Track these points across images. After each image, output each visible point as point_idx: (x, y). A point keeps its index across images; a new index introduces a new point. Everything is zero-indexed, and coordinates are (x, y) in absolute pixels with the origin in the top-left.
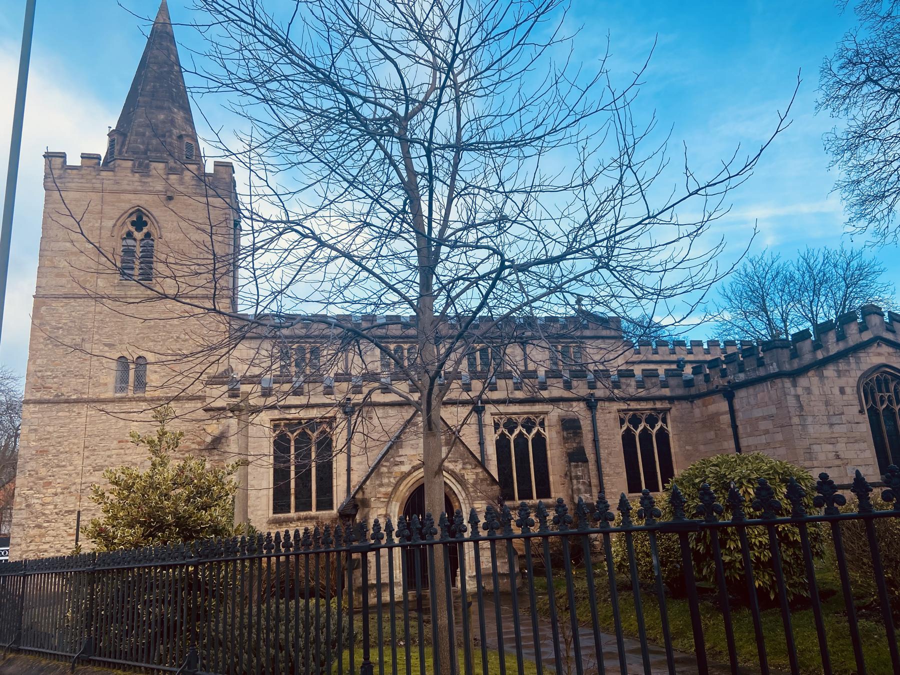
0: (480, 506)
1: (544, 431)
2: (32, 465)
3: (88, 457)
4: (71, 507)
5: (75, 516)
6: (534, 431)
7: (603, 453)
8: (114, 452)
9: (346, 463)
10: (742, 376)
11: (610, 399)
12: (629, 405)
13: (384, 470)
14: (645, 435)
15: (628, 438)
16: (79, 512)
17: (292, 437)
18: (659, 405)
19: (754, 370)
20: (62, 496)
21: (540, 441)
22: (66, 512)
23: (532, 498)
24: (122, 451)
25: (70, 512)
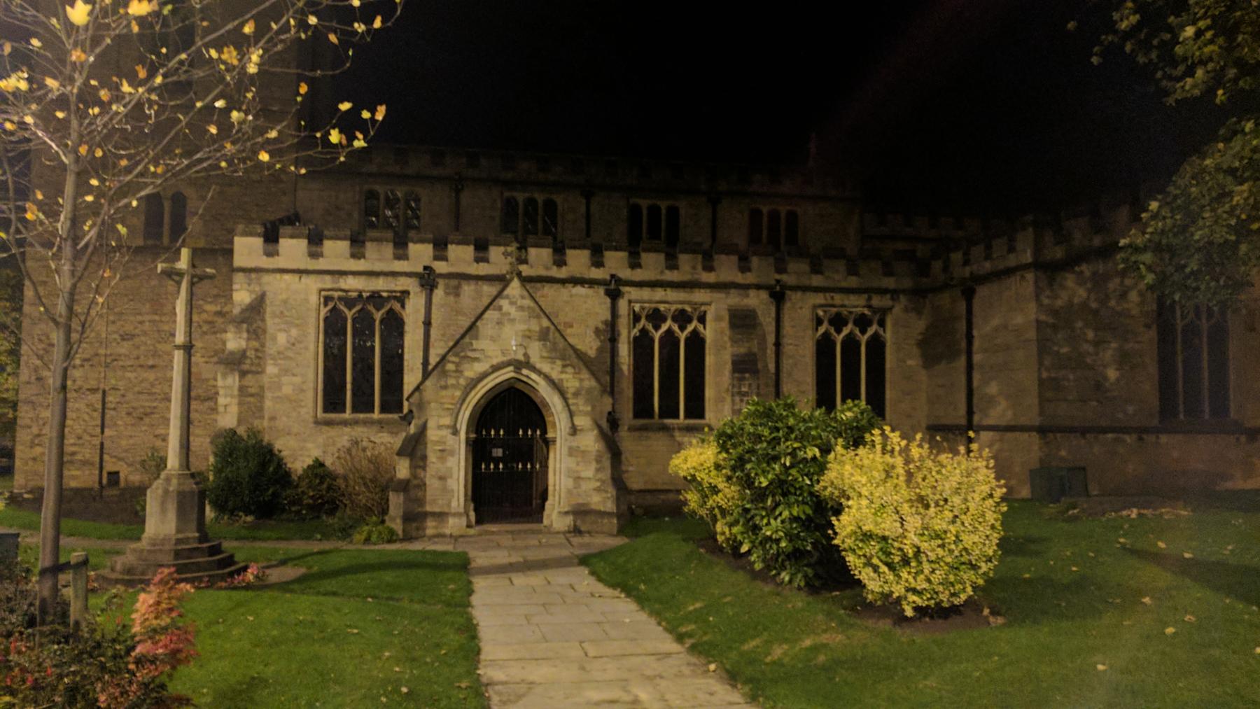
0: (583, 423)
2: (37, 330)
3: (113, 322)
4: (93, 384)
5: (99, 396)
6: (690, 328)
7: (786, 364)
8: (147, 318)
9: (421, 354)
10: (988, 265)
13: (450, 367)
15: (824, 348)
16: (104, 392)
17: (349, 314)
18: (877, 301)
20: (81, 369)
21: (696, 343)
22: (88, 390)
23: (677, 417)
24: (157, 318)
25: (93, 391)
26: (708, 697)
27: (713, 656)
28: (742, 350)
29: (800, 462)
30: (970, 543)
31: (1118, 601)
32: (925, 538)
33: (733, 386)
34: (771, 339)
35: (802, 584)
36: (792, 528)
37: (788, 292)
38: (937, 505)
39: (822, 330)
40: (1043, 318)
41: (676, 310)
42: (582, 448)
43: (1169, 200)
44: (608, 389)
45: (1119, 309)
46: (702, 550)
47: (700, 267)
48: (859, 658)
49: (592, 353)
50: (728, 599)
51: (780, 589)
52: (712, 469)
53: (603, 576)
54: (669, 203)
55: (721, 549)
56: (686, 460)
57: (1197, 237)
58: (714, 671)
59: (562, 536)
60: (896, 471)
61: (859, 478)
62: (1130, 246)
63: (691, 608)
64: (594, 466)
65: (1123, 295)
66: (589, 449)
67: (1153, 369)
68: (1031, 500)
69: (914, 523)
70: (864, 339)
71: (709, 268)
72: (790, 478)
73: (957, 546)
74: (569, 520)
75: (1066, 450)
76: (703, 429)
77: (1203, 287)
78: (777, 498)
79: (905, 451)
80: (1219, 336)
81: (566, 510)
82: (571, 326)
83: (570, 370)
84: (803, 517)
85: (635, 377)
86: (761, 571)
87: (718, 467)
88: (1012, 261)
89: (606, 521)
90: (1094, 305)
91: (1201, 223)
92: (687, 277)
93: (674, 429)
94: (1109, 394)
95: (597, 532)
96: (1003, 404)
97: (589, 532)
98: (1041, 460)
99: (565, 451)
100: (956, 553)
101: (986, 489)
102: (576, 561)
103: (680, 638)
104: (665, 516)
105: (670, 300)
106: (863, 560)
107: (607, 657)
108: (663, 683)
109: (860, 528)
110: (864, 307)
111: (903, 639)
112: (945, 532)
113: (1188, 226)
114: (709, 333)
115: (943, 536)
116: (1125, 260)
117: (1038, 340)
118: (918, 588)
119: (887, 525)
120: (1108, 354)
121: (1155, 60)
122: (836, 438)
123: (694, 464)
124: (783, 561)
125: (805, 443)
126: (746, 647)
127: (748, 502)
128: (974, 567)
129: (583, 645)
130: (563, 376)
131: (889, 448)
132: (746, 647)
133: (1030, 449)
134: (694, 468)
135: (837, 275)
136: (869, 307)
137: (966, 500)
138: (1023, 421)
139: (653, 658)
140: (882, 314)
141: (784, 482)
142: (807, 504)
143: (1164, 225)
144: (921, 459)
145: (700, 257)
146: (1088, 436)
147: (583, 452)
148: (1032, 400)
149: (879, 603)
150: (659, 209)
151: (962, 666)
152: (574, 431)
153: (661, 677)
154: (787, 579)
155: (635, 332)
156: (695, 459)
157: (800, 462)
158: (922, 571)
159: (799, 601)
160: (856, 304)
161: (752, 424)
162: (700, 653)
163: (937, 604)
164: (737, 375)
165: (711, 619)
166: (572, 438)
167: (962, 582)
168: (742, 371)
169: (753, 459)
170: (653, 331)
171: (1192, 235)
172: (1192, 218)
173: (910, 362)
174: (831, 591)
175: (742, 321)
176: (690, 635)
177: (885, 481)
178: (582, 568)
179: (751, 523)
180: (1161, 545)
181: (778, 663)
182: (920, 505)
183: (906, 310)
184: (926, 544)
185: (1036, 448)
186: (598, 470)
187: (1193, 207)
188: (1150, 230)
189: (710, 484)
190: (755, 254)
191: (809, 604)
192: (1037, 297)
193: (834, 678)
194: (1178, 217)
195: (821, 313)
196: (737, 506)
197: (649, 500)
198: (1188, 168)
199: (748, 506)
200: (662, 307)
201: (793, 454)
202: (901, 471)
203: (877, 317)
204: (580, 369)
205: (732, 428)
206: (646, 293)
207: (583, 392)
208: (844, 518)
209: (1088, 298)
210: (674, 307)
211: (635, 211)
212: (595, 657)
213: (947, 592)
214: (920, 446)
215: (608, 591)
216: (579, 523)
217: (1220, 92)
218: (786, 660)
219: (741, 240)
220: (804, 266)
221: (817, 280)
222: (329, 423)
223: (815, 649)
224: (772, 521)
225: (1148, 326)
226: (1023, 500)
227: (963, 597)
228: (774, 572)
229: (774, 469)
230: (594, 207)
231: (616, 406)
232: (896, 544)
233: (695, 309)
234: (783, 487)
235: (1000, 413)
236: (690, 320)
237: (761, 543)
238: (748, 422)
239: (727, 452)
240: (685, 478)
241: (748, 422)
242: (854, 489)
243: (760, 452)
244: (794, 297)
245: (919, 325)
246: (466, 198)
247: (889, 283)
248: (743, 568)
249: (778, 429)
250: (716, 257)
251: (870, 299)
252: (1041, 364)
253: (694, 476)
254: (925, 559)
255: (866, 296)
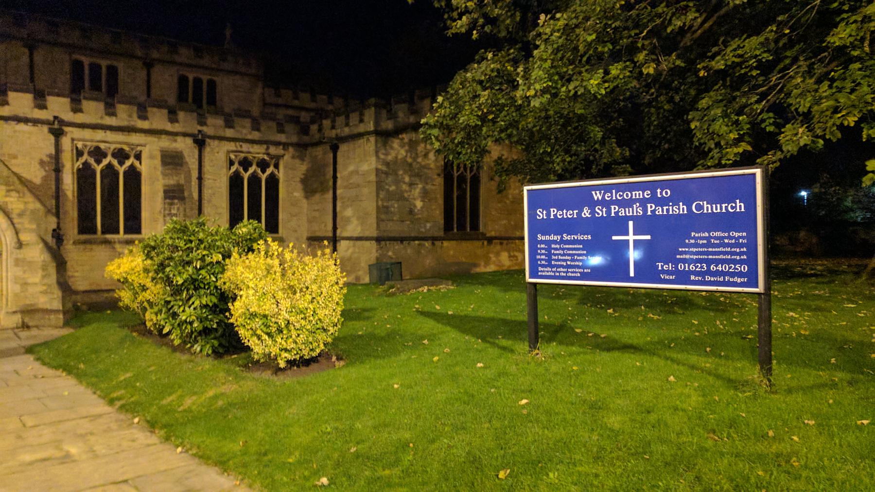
0: (29, 239)
1: (278, 172)
6: (128, 163)
7: (206, 193)
11: (221, 139)
12: (241, 146)
14: (254, 181)
15: (235, 182)
18: (273, 150)
19: (356, 125)
21: (133, 176)
23: (118, 232)
26: (130, 443)
27: (137, 412)
28: (172, 182)
29: (208, 265)
30: (323, 315)
31: (410, 344)
32: (293, 314)
33: (165, 209)
34: (195, 174)
35: (210, 352)
36: (202, 313)
37: (208, 140)
38: (301, 290)
39: (233, 169)
40: (380, 167)
41: (115, 149)
42: (28, 259)
43: (449, 96)
44: (54, 211)
45: (423, 163)
46: (134, 334)
47: (135, 116)
48: (246, 400)
49: (38, 181)
50: (152, 368)
51: (193, 357)
52: (141, 272)
53: (47, 360)
54: (109, 62)
55: (150, 332)
56: (119, 267)
57: (461, 121)
58: (138, 423)
59: (10, 331)
60: (274, 269)
61: (248, 275)
62: (426, 124)
63: (122, 378)
64: (40, 273)
65: (426, 155)
66: (36, 259)
67: (441, 201)
68: (370, 284)
69: (285, 304)
70: (264, 177)
71: (143, 117)
72: (201, 277)
73: (314, 318)
74: (17, 319)
75: (393, 251)
76: (134, 242)
77: (464, 152)
78: (191, 292)
79: (280, 256)
80: (476, 181)
81: (14, 310)
82: (15, 157)
83: (14, 194)
84: (211, 305)
85: (79, 202)
86: (179, 345)
87: (146, 270)
88: (361, 128)
89: (52, 317)
90: (409, 160)
91: (463, 113)
92: (124, 123)
93: (115, 242)
94: (416, 217)
95: (43, 326)
96: (355, 222)
97: (37, 327)
98: (377, 259)
99: (11, 262)
100: (314, 322)
101: (334, 279)
102: (23, 350)
103: (111, 402)
104: (106, 309)
105: (111, 141)
106: (251, 332)
107: (45, 424)
108: (92, 439)
109: (248, 310)
110: (264, 154)
111: (278, 383)
112: (307, 309)
113: (458, 114)
114: (144, 168)
115: (305, 312)
116: (424, 133)
117: (377, 182)
118: (288, 348)
119: (267, 307)
120: (417, 191)
121: (444, 7)
122: (234, 247)
123: (126, 269)
124: (195, 337)
125: (212, 251)
126: (164, 402)
127: (168, 296)
128: (325, 330)
129: (22, 418)
130: (7, 199)
131: (270, 253)
132: (164, 402)
133: (369, 253)
134: (126, 272)
135: (244, 129)
136: (268, 154)
137: (320, 287)
138: (367, 234)
139: (87, 420)
140: (277, 159)
141: (196, 280)
142: (213, 295)
143: (445, 112)
144: (292, 260)
145: (135, 108)
146: (404, 242)
147: (30, 262)
148: (372, 220)
149: (262, 361)
150: (99, 67)
151: (314, 397)
152: (20, 245)
153: (92, 434)
154: (199, 349)
155: (79, 164)
156: (127, 265)
157: (208, 265)
158: (291, 337)
159: (208, 364)
160: (258, 152)
161: (171, 238)
162: (127, 411)
163: (301, 357)
164: (168, 201)
165: (138, 384)
166: (18, 251)
167: (317, 341)
168: (173, 198)
169: (171, 264)
170: (95, 165)
171: (459, 120)
172: (460, 109)
173: (296, 194)
174: (231, 355)
175: (172, 160)
176: (119, 399)
177: (266, 276)
178: (28, 356)
179: (171, 311)
180: (438, 307)
181: (189, 411)
182: (290, 292)
183: (293, 157)
184: (293, 318)
185: (374, 251)
186: (44, 277)
187: (461, 103)
188: (437, 115)
189: (140, 284)
190: (182, 109)
191: (214, 365)
192: (377, 152)
193: (228, 416)
194: (452, 108)
195: (233, 157)
196: (161, 299)
197: (94, 298)
198: (458, 77)
199: (168, 299)
200: (102, 146)
201: (203, 259)
202: (279, 269)
203: (273, 162)
204: (24, 194)
205: (155, 241)
206: (87, 134)
207: (28, 213)
208: (237, 304)
209: (406, 156)
210: (113, 147)
211: (77, 67)
212: (31, 427)
213: (308, 348)
214: (292, 252)
215: (50, 372)
216: (26, 320)
217: (475, 32)
218: (194, 407)
219: (172, 100)
220: (220, 122)
221: (229, 133)
222: (85, 242)
223: (216, 397)
224: (187, 309)
225: (439, 175)
226: (365, 285)
227: (318, 351)
228: (189, 345)
229: (188, 271)
230: (38, 58)
231: (61, 225)
232: (273, 320)
233: (132, 149)
234: (195, 284)
235: (352, 228)
236: (127, 157)
237: (179, 325)
238: (168, 237)
239: (152, 258)
240: (119, 280)
241: (168, 237)
242: (244, 283)
243: (177, 259)
244: (212, 144)
245: (302, 168)
246: (39, 57)
247: (282, 138)
248: (166, 344)
249: (191, 242)
250: (149, 109)
251: (268, 148)
252: (378, 196)
253: (126, 279)
254: (293, 328)
255: (265, 146)
